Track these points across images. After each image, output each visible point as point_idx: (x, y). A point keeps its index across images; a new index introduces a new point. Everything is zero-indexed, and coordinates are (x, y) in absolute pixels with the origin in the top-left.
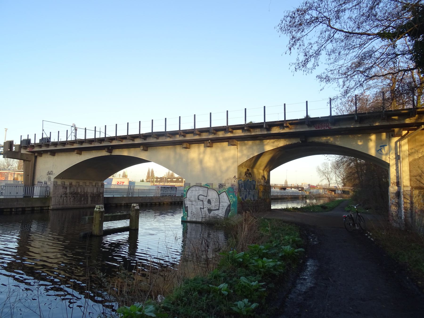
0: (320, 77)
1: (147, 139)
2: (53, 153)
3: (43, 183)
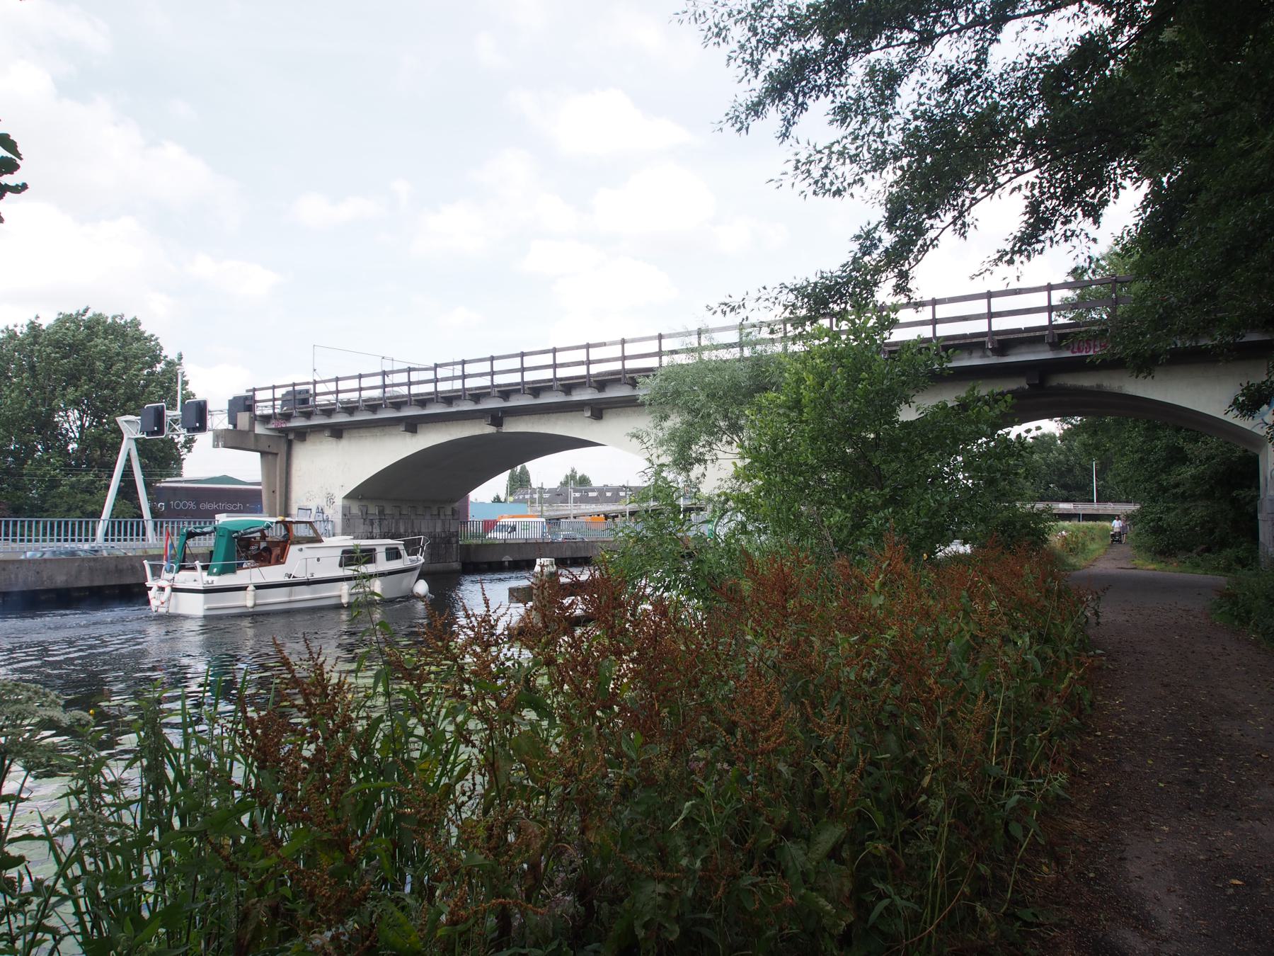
0: (1096, 221)
1: (574, 393)
2: (337, 432)
3: (314, 511)
